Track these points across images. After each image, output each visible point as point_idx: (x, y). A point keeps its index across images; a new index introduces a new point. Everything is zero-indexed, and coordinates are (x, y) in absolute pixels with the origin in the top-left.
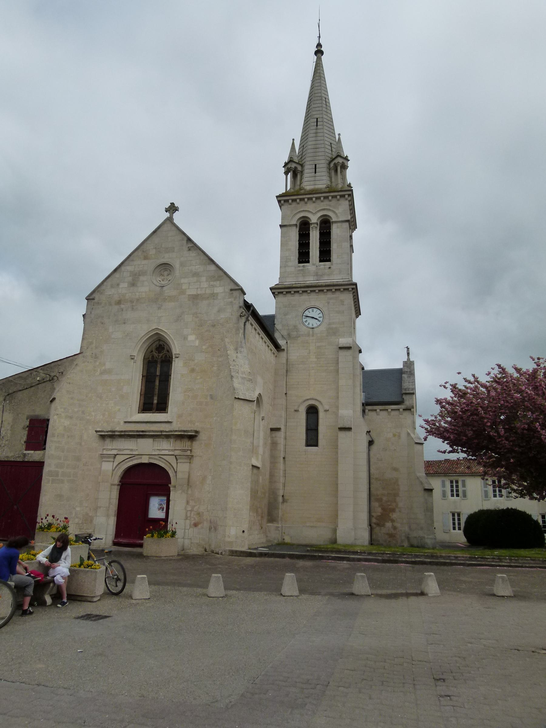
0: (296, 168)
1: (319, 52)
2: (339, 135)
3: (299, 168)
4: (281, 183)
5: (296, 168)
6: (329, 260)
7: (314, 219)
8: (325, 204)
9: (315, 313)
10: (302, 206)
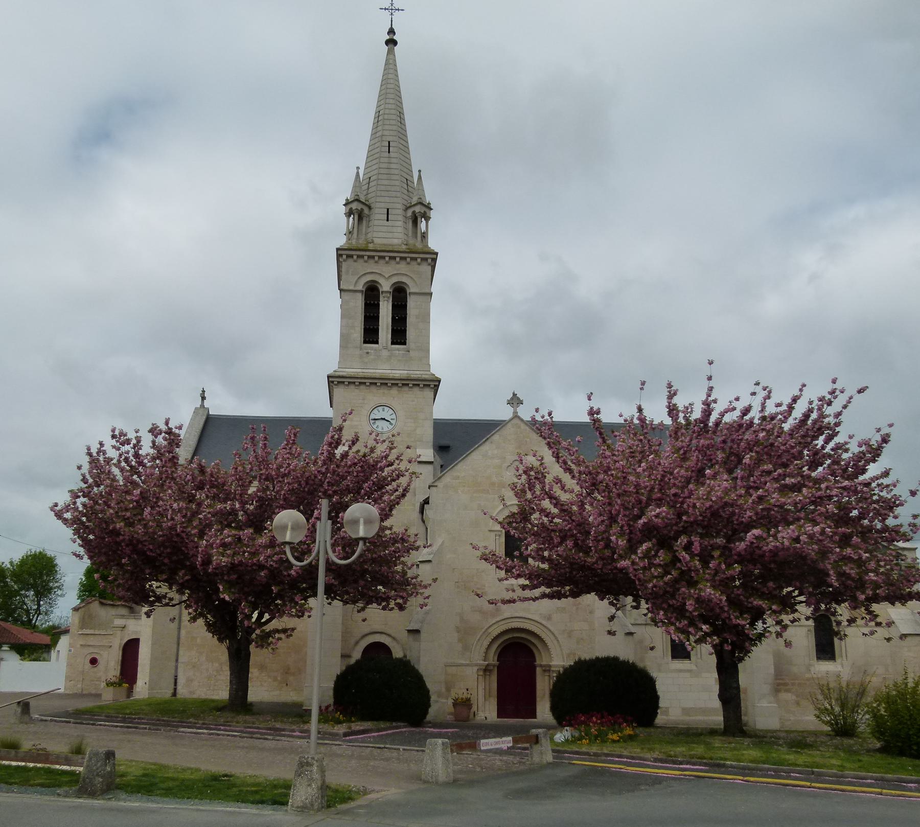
2: (420, 171)
3: (366, 211)
4: (336, 228)
6: (405, 344)
7: (386, 286)
8: (403, 267)
9: (387, 414)
10: (371, 267)
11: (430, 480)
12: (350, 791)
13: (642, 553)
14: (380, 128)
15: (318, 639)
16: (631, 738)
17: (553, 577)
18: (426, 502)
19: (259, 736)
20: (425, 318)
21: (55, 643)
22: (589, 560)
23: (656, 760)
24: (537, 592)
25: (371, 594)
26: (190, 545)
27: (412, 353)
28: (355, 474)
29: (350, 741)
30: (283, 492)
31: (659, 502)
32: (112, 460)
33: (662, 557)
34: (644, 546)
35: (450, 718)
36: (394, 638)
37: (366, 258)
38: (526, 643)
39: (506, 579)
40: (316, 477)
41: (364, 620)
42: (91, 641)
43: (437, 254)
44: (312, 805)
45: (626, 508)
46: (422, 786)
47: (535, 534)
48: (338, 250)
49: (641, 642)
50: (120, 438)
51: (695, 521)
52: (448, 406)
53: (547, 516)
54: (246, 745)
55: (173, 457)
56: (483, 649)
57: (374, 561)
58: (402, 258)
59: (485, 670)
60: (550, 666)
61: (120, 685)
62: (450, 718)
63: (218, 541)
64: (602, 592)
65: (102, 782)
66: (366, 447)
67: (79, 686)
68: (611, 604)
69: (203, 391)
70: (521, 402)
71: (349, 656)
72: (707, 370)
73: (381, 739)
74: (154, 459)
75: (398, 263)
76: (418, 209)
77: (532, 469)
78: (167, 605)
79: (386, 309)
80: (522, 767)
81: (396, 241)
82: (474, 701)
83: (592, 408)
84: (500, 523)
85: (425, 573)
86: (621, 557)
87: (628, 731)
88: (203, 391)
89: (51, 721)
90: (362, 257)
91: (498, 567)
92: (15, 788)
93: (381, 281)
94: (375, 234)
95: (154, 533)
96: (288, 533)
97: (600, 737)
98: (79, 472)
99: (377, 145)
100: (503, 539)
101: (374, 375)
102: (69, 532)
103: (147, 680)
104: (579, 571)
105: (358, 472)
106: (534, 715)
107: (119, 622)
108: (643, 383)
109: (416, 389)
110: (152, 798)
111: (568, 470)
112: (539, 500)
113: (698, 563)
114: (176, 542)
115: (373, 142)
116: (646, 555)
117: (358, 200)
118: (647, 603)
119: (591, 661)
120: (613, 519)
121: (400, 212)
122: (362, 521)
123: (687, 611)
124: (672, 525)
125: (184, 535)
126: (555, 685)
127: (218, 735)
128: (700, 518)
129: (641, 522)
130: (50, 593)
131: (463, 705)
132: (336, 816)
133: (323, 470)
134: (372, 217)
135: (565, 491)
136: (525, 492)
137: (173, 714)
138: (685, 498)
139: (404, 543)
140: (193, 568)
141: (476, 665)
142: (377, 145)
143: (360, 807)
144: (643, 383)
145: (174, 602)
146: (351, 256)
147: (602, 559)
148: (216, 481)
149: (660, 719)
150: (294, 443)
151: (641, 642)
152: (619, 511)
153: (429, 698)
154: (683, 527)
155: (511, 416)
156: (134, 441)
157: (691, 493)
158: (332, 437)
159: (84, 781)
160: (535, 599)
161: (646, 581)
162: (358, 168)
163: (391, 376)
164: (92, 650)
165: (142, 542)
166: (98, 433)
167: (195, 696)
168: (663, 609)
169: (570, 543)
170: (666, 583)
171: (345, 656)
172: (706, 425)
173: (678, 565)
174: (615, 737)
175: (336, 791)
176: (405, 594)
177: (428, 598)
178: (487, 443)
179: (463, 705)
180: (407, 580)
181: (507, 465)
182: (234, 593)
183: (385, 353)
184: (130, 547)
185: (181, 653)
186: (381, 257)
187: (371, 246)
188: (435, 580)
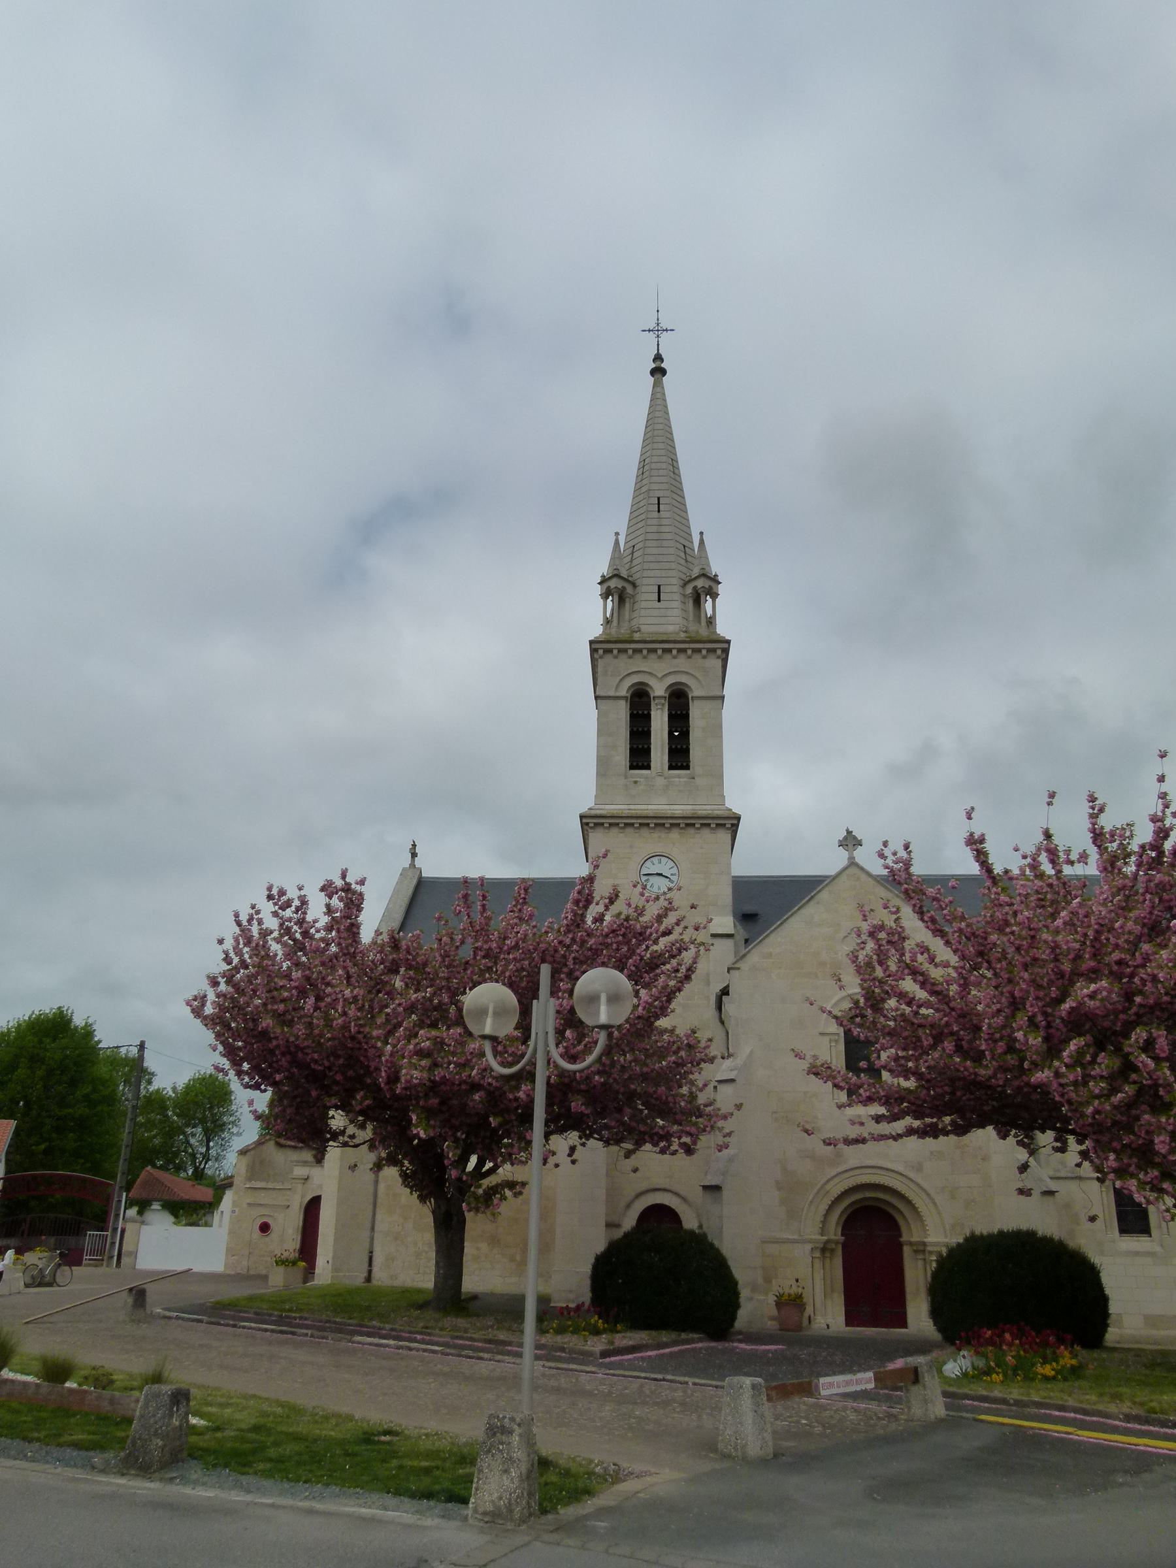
0: (624, 588)
1: (658, 372)
2: (701, 533)
3: (629, 589)
4: (590, 616)
5: (624, 588)
6: (687, 767)
7: (659, 689)
8: (681, 663)
9: (665, 867)
10: (638, 664)
11: (730, 959)
12: (591, 1474)
13: (1070, 1057)
14: (645, 482)
15: (564, 1201)
16: (1075, 1372)
17: (925, 1101)
18: (725, 992)
19: (470, 1353)
20: (716, 730)
21: (218, 1199)
22: (982, 1072)
23: (1128, 1418)
24: (899, 1126)
25: (642, 1128)
26: (371, 1052)
27: (698, 781)
28: (615, 946)
29: (610, 1366)
30: (507, 974)
31: (1093, 975)
32: (271, 932)
33: (1106, 1063)
34: (1073, 1045)
35: (772, 1325)
36: (684, 1199)
37: (630, 652)
38: (891, 1211)
39: (849, 1105)
40: (556, 951)
41: (635, 1170)
42: (262, 1198)
43: (728, 642)
44: (511, 1511)
45: (1040, 987)
46: (718, 1466)
47: (891, 1033)
48: (591, 642)
49: (1067, 1206)
50: (276, 897)
51: (1158, 1005)
52: (754, 856)
53: (909, 1004)
54: (446, 1369)
55: (352, 925)
56: (819, 1218)
57: (645, 1077)
58: (680, 651)
59: (823, 1250)
60: (924, 1244)
61: (294, 1263)
62: (772, 1325)
63: (411, 1047)
64: (1004, 1124)
65: (163, 1448)
66: (629, 905)
67: (245, 1263)
68: (1020, 1143)
69: (414, 845)
70: (859, 843)
71: (618, 1226)
72: (1158, 768)
73: (658, 1365)
74: (329, 929)
75: (675, 657)
76: (700, 583)
77: (881, 927)
78: (345, 1145)
79: (659, 714)
80: (893, 1426)
81: (671, 628)
82: (807, 1298)
83: (972, 834)
84: (836, 1017)
85: (725, 1098)
86: (1035, 1065)
87: (1067, 1359)
88: (414, 845)
89: (178, 1318)
90: (625, 651)
91: (836, 1086)
92: (30, 1449)
93: (651, 682)
94: (642, 621)
95: (321, 1035)
96: (489, 1021)
97: (1022, 1372)
98: (220, 948)
99: (642, 504)
100: (842, 1047)
101: (645, 813)
102: (209, 1036)
103: (330, 1257)
104: (965, 1095)
105: (618, 943)
106: (903, 1323)
107: (300, 1171)
108: (1052, 795)
109: (706, 831)
110: (244, 1479)
111: (939, 932)
112: (897, 980)
113: (1168, 1073)
114: (352, 1049)
115: (638, 499)
116: (1078, 1061)
117: (617, 576)
118: (1080, 1142)
119: (991, 1236)
120: (1016, 1005)
121: (675, 589)
122: (603, 998)
123: (1158, 1153)
124: (1116, 1012)
125: (360, 1036)
126: (935, 1275)
127: (410, 1349)
128: (1166, 998)
129: (1066, 1006)
130: (223, 1131)
131: (791, 1304)
132: (555, 1537)
133: (568, 941)
134: (638, 598)
135: (936, 966)
136: (874, 969)
137: (358, 1313)
138: (1136, 967)
139: (691, 1054)
140: (375, 1089)
141: (810, 1241)
142: (642, 504)
143: (602, 1512)
144: (1052, 795)
145: (357, 1141)
146: (610, 651)
147: (1004, 1069)
148: (414, 959)
149: (1112, 1335)
150: (525, 903)
151: (1067, 1206)
152: (1028, 992)
153: (737, 1294)
154: (1136, 1014)
155: (845, 862)
156: (297, 903)
157: (1147, 959)
158: (579, 892)
159: (134, 1443)
160: (897, 1137)
161: (1081, 1104)
162: (617, 534)
163: (669, 813)
164: (263, 1211)
165: (302, 1049)
166: (249, 896)
167: (397, 1283)
168: (1114, 1151)
169: (949, 1045)
170: (1115, 1107)
171: (610, 1225)
172: (1161, 853)
173: (1134, 1076)
174: (1048, 1370)
175: (567, 1473)
176: (693, 1130)
177: (729, 1134)
178: (812, 903)
179: (791, 1304)
180: (698, 1109)
181: (842, 935)
182: (434, 1127)
183: (660, 782)
184: (288, 1057)
185: (379, 1217)
186: (651, 651)
187: (637, 636)
188: (739, 1107)
